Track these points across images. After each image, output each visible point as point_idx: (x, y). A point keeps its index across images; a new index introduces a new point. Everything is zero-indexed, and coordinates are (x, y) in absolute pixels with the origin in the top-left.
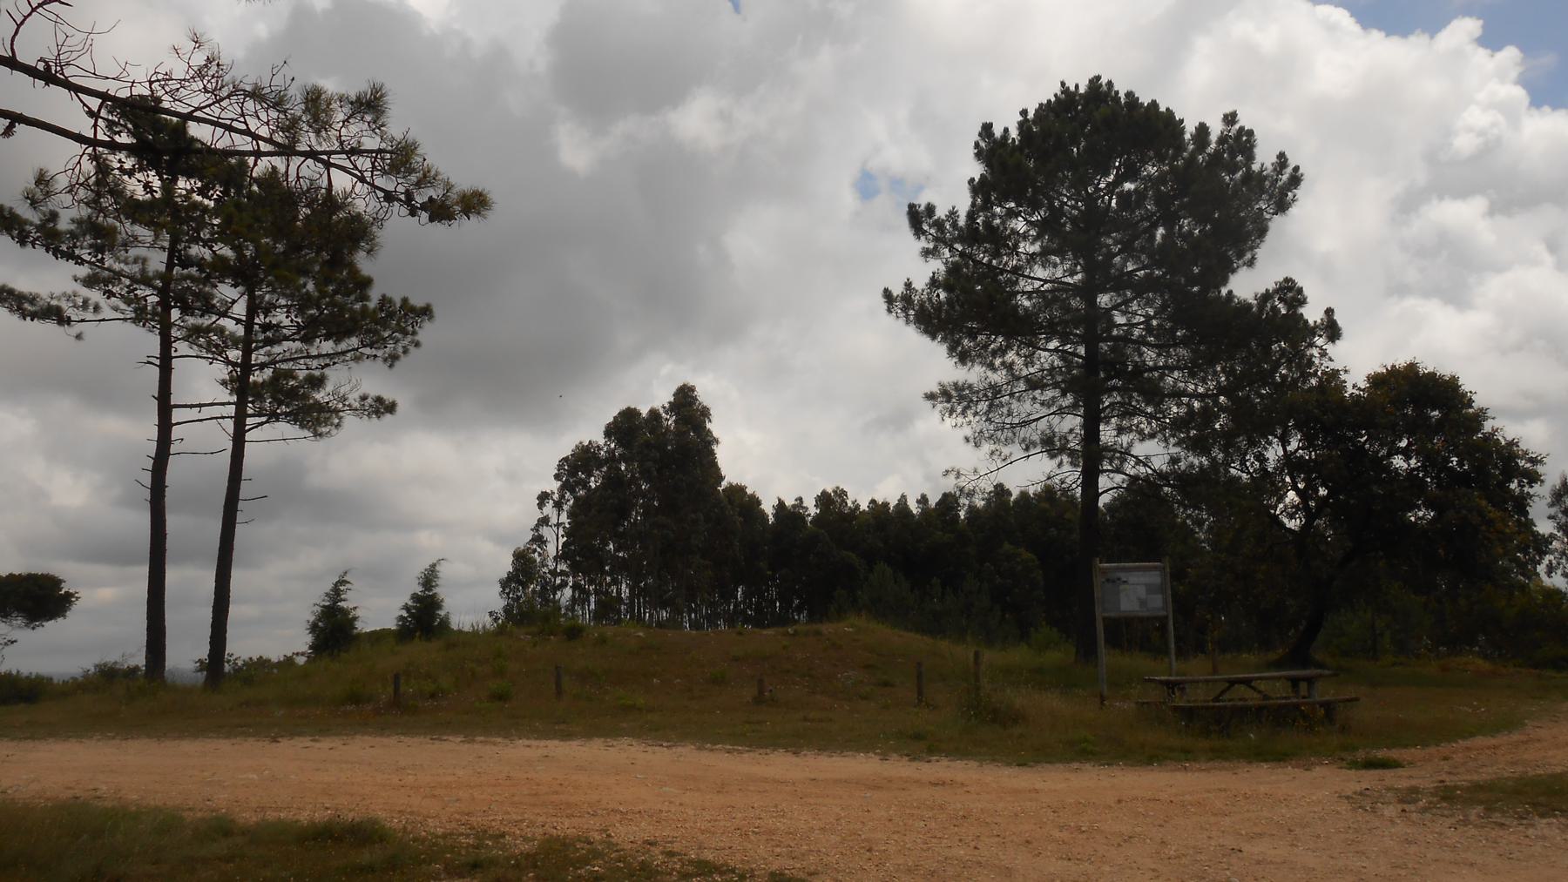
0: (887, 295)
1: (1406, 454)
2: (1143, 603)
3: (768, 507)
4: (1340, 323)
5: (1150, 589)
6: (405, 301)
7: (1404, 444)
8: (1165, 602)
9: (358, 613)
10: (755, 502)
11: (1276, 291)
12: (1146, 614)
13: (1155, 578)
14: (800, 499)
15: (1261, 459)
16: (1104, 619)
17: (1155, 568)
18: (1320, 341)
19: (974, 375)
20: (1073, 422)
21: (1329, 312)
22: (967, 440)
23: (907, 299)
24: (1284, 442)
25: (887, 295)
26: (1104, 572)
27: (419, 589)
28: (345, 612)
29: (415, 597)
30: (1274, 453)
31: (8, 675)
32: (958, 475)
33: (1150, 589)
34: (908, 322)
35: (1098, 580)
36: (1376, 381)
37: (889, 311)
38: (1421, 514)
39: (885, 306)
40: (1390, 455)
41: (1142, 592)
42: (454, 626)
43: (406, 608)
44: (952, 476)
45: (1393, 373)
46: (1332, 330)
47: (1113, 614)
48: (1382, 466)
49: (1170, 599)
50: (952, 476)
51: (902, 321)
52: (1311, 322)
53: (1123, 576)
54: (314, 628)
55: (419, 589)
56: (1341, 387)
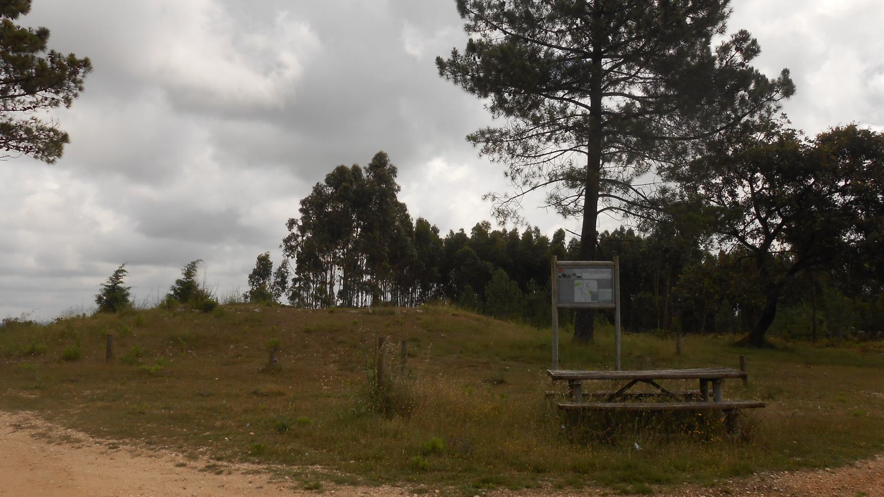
0: (439, 61)
1: (843, 191)
2: (594, 296)
3: (443, 235)
4: (794, 82)
5: (601, 283)
6: (72, 55)
7: (842, 184)
8: (614, 295)
9: (129, 291)
10: (436, 230)
11: (734, 42)
12: (596, 306)
13: (606, 274)
14: (462, 230)
15: (733, 194)
16: (559, 309)
17: (607, 266)
18: (777, 96)
19: (505, 123)
20: (581, 161)
21: (786, 72)
22: (506, 174)
23: (452, 63)
24: (752, 181)
25: (439, 61)
26: (560, 267)
27: (182, 277)
28: (120, 289)
29: (179, 282)
30: (743, 193)
31: (11, 324)
32: (494, 198)
33: (601, 283)
34: (456, 82)
35: (555, 275)
36: (824, 139)
37: (441, 74)
38: (851, 237)
39: (438, 71)
40: (831, 193)
41: (594, 286)
42: (130, 299)
43: (174, 289)
44: (489, 199)
45: (837, 133)
46: (787, 86)
47: (566, 305)
48: (825, 202)
49: (618, 293)
50: (489, 199)
51: (451, 82)
52: (770, 80)
53: (578, 272)
54: (99, 299)
55: (182, 277)
56: (796, 145)
